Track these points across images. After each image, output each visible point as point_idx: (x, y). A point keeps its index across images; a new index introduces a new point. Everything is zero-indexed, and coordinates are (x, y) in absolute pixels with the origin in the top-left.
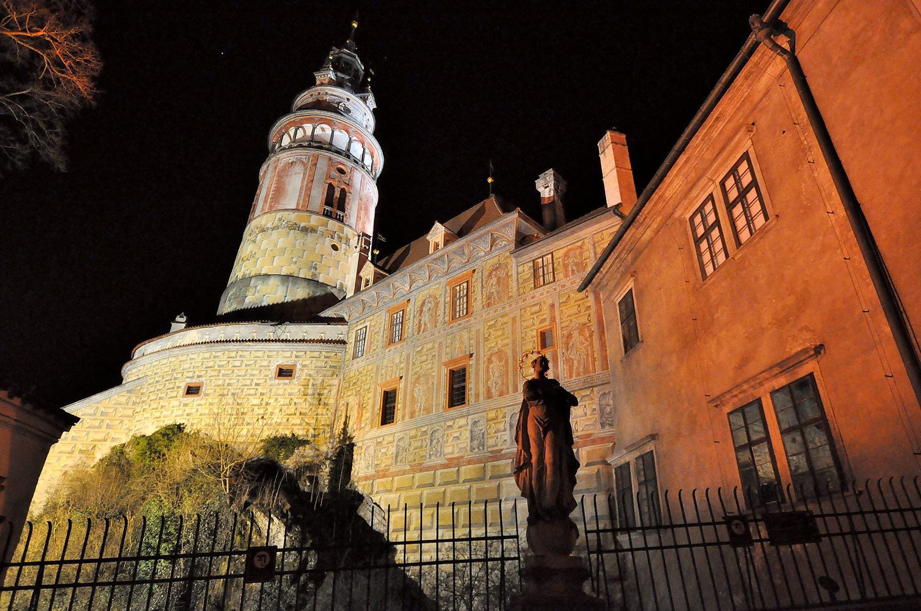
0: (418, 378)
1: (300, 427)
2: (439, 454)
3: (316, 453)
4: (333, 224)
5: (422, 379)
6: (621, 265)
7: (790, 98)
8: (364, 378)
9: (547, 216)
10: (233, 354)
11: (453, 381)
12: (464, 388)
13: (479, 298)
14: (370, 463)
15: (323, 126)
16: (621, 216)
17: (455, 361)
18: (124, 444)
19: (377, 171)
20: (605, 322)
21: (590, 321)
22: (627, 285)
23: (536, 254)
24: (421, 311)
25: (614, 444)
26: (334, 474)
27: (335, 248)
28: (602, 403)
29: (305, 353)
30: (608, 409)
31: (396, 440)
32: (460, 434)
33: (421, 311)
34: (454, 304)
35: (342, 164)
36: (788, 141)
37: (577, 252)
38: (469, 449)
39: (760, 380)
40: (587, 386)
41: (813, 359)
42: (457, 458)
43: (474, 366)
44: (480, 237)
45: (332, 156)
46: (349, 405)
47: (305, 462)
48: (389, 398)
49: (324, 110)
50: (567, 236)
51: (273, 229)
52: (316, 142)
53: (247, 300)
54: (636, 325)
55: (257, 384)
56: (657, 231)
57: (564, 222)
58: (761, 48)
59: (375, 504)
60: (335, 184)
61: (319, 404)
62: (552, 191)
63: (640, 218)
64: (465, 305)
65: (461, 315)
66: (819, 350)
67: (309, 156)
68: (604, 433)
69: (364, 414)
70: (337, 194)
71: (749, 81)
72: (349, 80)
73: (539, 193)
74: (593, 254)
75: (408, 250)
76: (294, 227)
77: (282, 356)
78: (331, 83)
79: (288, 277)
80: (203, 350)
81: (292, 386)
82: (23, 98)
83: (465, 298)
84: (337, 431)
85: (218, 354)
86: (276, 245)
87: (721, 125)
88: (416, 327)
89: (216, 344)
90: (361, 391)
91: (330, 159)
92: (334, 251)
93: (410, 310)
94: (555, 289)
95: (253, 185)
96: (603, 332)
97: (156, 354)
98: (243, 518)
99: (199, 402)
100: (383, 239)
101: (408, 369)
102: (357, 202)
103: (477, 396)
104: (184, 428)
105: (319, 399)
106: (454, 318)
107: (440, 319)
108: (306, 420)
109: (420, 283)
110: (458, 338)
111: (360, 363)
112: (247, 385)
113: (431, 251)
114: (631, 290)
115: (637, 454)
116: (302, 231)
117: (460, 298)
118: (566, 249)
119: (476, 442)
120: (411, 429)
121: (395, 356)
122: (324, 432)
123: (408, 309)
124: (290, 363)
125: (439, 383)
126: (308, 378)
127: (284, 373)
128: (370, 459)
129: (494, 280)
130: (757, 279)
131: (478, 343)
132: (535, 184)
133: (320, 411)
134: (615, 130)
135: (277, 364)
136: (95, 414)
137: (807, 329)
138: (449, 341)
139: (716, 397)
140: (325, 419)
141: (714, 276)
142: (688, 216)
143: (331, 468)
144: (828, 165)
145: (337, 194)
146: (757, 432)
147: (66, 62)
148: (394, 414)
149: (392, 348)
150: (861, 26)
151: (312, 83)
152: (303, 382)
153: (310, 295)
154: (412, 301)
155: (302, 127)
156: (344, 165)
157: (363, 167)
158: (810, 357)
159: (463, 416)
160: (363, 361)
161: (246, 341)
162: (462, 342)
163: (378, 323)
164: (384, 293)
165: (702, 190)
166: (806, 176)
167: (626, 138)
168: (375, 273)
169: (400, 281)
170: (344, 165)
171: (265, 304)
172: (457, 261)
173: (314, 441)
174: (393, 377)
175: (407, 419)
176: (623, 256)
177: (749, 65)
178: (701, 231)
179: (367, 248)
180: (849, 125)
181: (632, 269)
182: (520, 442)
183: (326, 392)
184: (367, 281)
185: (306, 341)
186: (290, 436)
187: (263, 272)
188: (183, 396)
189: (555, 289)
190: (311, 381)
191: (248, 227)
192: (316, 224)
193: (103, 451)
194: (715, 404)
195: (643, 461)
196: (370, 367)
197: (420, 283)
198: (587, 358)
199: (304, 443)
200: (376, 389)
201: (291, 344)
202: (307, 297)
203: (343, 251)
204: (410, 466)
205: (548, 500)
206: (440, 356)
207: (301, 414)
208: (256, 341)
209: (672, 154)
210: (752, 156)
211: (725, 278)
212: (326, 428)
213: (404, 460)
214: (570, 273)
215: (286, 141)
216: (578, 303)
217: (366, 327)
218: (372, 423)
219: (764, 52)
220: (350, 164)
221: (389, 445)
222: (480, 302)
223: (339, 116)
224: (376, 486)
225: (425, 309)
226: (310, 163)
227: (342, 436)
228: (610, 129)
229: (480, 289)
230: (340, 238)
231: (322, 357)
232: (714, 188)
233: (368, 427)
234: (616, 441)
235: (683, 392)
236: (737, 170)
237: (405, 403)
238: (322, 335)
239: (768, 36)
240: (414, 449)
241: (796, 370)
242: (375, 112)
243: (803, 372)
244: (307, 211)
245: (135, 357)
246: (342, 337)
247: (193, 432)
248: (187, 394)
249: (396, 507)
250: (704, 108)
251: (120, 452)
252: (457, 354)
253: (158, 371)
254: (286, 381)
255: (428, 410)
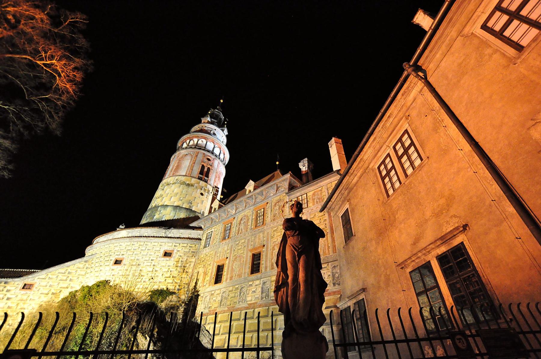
0: (236, 258)
1: (171, 284)
2: (244, 301)
3: (178, 299)
4: (202, 183)
5: (238, 258)
6: (342, 197)
7: (427, 100)
8: (208, 258)
9: (304, 179)
10: (142, 243)
11: (254, 260)
12: (259, 263)
13: (269, 216)
14: (207, 306)
15: (202, 139)
16: (340, 175)
17: (255, 249)
18: (77, 291)
19: (226, 162)
20: (334, 227)
21: (326, 227)
22: (345, 206)
23: (298, 194)
24: (240, 223)
25: (341, 295)
26: (186, 313)
27: (202, 194)
28: (334, 271)
29: (180, 244)
30: (337, 275)
31: (221, 293)
32: (256, 289)
33: (240, 223)
34: (256, 219)
35: (210, 156)
36: (429, 119)
37: (319, 193)
38: (260, 298)
39: (429, 250)
40: (325, 262)
41: (461, 234)
42: (254, 303)
43: (265, 252)
44: (271, 186)
45: (205, 152)
46: (199, 273)
47: (172, 305)
48: (220, 269)
49: (203, 133)
50: (313, 185)
51: (173, 184)
52: (198, 146)
53: (155, 218)
54: (351, 227)
55: (152, 260)
56: (360, 178)
57: (312, 180)
58: (412, 77)
59: (207, 330)
60: (205, 165)
61: (184, 272)
62: (307, 168)
63: (351, 171)
64: (262, 220)
65: (260, 225)
66: (465, 227)
67: (194, 152)
68: (335, 289)
69: (206, 278)
70: (206, 170)
71: (404, 96)
72: (217, 122)
73: (301, 169)
74: (327, 194)
75: (237, 195)
76: (183, 183)
77: (167, 245)
78: (208, 122)
79: (177, 206)
80: (127, 242)
81: (170, 262)
82: (47, 100)
83: (262, 217)
84: (191, 287)
85: (134, 243)
86: (173, 192)
87: (391, 120)
88: (237, 231)
89: (134, 238)
90: (206, 265)
91: (204, 154)
92: (201, 196)
93: (235, 223)
94: (308, 211)
95: (168, 163)
96: (333, 233)
97: (103, 242)
98: (130, 336)
99: (120, 269)
100: (225, 191)
101: (231, 253)
102: (215, 174)
103: (266, 268)
104: (110, 282)
105: (184, 269)
106: (256, 226)
107: (249, 227)
108: (175, 281)
109: (241, 209)
110: (258, 236)
111: (207, 250)
112: (146, 260)
113: (247, 193)
114: (348, 209)
115: (354, 301)
116: (187, 185)
117: (260, 217)
118: (313, 191)
119: (264, 294)
120: (229, 287)
121: (225, 247)
122: (184, 288)
123: (234, 222)
124: (171, 249)
125: (246, 261)
126: (179, 257)
127: (167, 254)
128: (207, 304)
129: (277, 207)
130: (420, 192)
131: (268, 239)
132: (298, 165)
133: (183, 276)
134: (337, 138)
135: (165, 249)
136: (65, 273)
137: (455, 216)
138: (253, 239)
139: (402, 262)
140: (185, 281)
141: (394, 194)
142: (376, 167)
143: (185, 308)
144: (455, 125)
145: (206, 170)
146: (429, 282)
147: (62, 73)
148: (222, 278)
149: (224, 242)
150: (462, 58)
151: (200, 122)
152: (176, 259)
153: (187, 216)
154: (236, 219)
155: (193, 140)
156: (210, 157)
157: (219, 159)
158: (460, 232)
159: (258, 279)
160: (208, 249)
161: (150, 237)
162: (259, 239)
163: (217, 230)
164: (223, 215)
165: (383, 152)
166: (442, 134)
167: (342, 141)
168: (219, 205)
169: (231, 208)
170: (210, 157)
171: (164, 219)
172: (260, 198)
173: (178, 292)
174: (223, 257)
175: (228, 281)
176: (342, 192)
177: (405, 86)
178: (384, 173)
179: (217, 193)
180: (464, 104)
181: (348, 198)
182: (280, 266)
183: (188, 265)
184: (215, 209)
185: (181, 238)
186: (165, 289)
187: (165, 204)
188: (112, 265)
189: (308, 211)
190: (181, 259)
191: (161, 183)
192: (194, 182)
193: (65, 294)
194: (401, 267)
195: (358, 305)
196: (212, 252)
197: (241, 209)
198: (325, 247)
199: (173, 293)
200: (213, 264)
201: (173, 239)
202: (185, 217)
203: (206, 196)
204: (228, 308)
205: (301, 314)
206: (248, 247)
207: (173, 277)
208: (155, 237)
209: (367, 135)
210: (410, 131)
211: (401, 195)
212: (186, 285)
213: (225, 304)
214: (316, 203)
215: (185, 145)
216: (320, 218)
217: (212, 232)
218: (209, 283)
219: (411, 81)
220: (213, 157)
221: (218, 295)
222: (270, 218)
223: (210, 136)
224: (208, 320)
225: (242, 222)
226: (194, 155)
227: (193, 290)
228: (334, 137)
229: (270, 212)
230: (205, 190)
231: (188, 247)
232: (390, 151)
233: (207, 286)
234: (342, 293)
235: (380, 261)
236: (402, 140)
237: (228, 272)
238: (190, 235)
239: (413, 70)
240: (231, 298)
241: (451, 242)
242: (227, 136)
243: (456, 242)
244: (190, 176)
245: (94, 243)
246: (199, 237)
247: (114, 285)
248: (115, 264)
249: (218, 332)
250: (382, 110)
251: (73, 295)
252: (257, 245)
253: (103, 251)
254: (168, 258)
255: (240, 276)
